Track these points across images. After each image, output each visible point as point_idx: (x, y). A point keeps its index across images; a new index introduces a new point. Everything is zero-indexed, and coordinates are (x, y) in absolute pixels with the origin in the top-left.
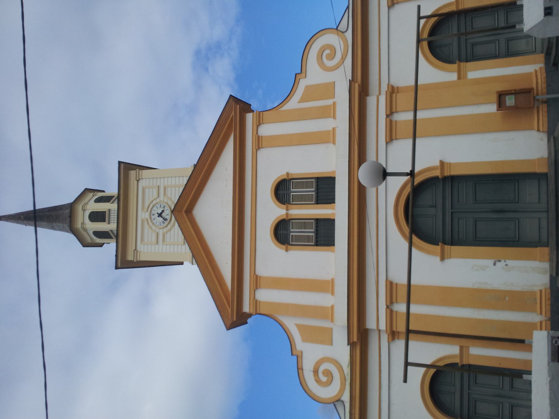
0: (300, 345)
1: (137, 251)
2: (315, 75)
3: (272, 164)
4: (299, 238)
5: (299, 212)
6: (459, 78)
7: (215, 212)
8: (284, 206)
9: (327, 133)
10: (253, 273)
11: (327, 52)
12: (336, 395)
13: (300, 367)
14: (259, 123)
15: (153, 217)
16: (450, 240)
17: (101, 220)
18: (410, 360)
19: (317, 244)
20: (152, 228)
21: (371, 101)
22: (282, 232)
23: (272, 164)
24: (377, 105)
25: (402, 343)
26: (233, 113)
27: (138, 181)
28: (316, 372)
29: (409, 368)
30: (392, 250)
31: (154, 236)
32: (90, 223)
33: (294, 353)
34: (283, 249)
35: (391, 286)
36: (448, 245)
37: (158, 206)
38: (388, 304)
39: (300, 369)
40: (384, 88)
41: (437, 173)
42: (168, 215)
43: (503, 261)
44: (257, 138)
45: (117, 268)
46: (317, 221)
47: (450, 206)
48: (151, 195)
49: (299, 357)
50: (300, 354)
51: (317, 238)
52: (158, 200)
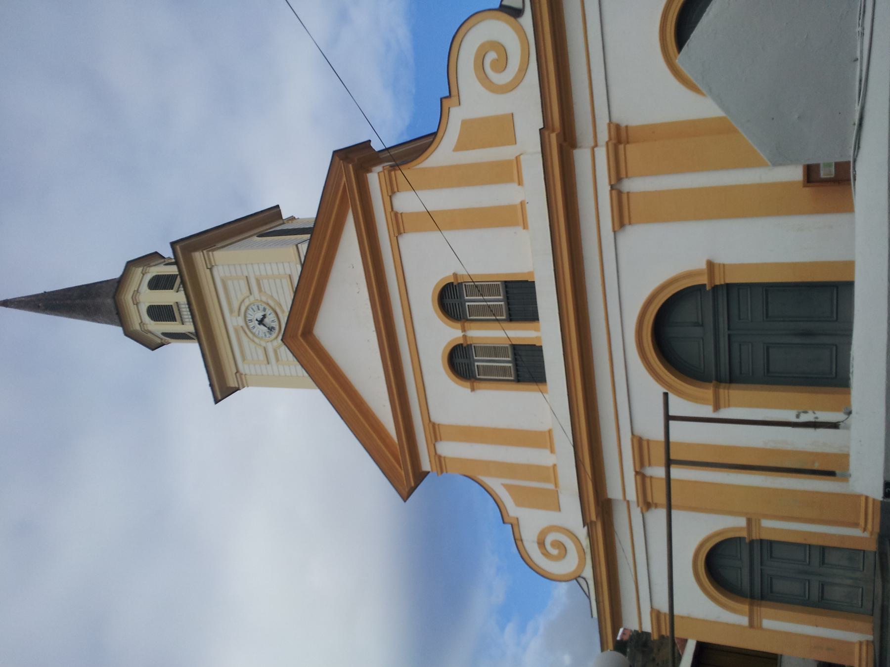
0: (513, 510)
1: (241, 374)
2: (475, 102)
3: (426, 263)
4: (488, 370)
5: (486, 334)
6: (751, 625)
7: (347, 325)
8: (459, 325)
9: (511, 208)
10: (427, 421)
11: (492, 56)
12: (575, 571)
13: (517, 536)
14: (391, 190)
15: (251, 325)
16: (728, 374)
17: (162, 296)
18: (671, 413)
19: (519, 379)
20: (253, 341)
21: (582, 157)
22: (461, 362)
23: (426, 263)
24: (592, 165)
25: (662, 513)
26: (344, 179)
27: (211, 269)
28: (541, 544)
29: (672, 423)
30: (638, 395)
31: (260, 352)
32: (152, 322)
33: (506, 520)
34: (457, 328)
35: (640, 444)
36: (726, 382)
37: (255, 308)
38: (638, 470)
39: (518, 540)
40: (604, 135)
41: (704, 280)
42: (273, 321)
43: (810, 412)
44: (393, 218)
45: (217, 401)
46: (515, 347)
47: (726, 326)
48: (238, 292)
49: (515, 526)
50: (515, 522)
51: (517, 370)
52: (252, 299)
